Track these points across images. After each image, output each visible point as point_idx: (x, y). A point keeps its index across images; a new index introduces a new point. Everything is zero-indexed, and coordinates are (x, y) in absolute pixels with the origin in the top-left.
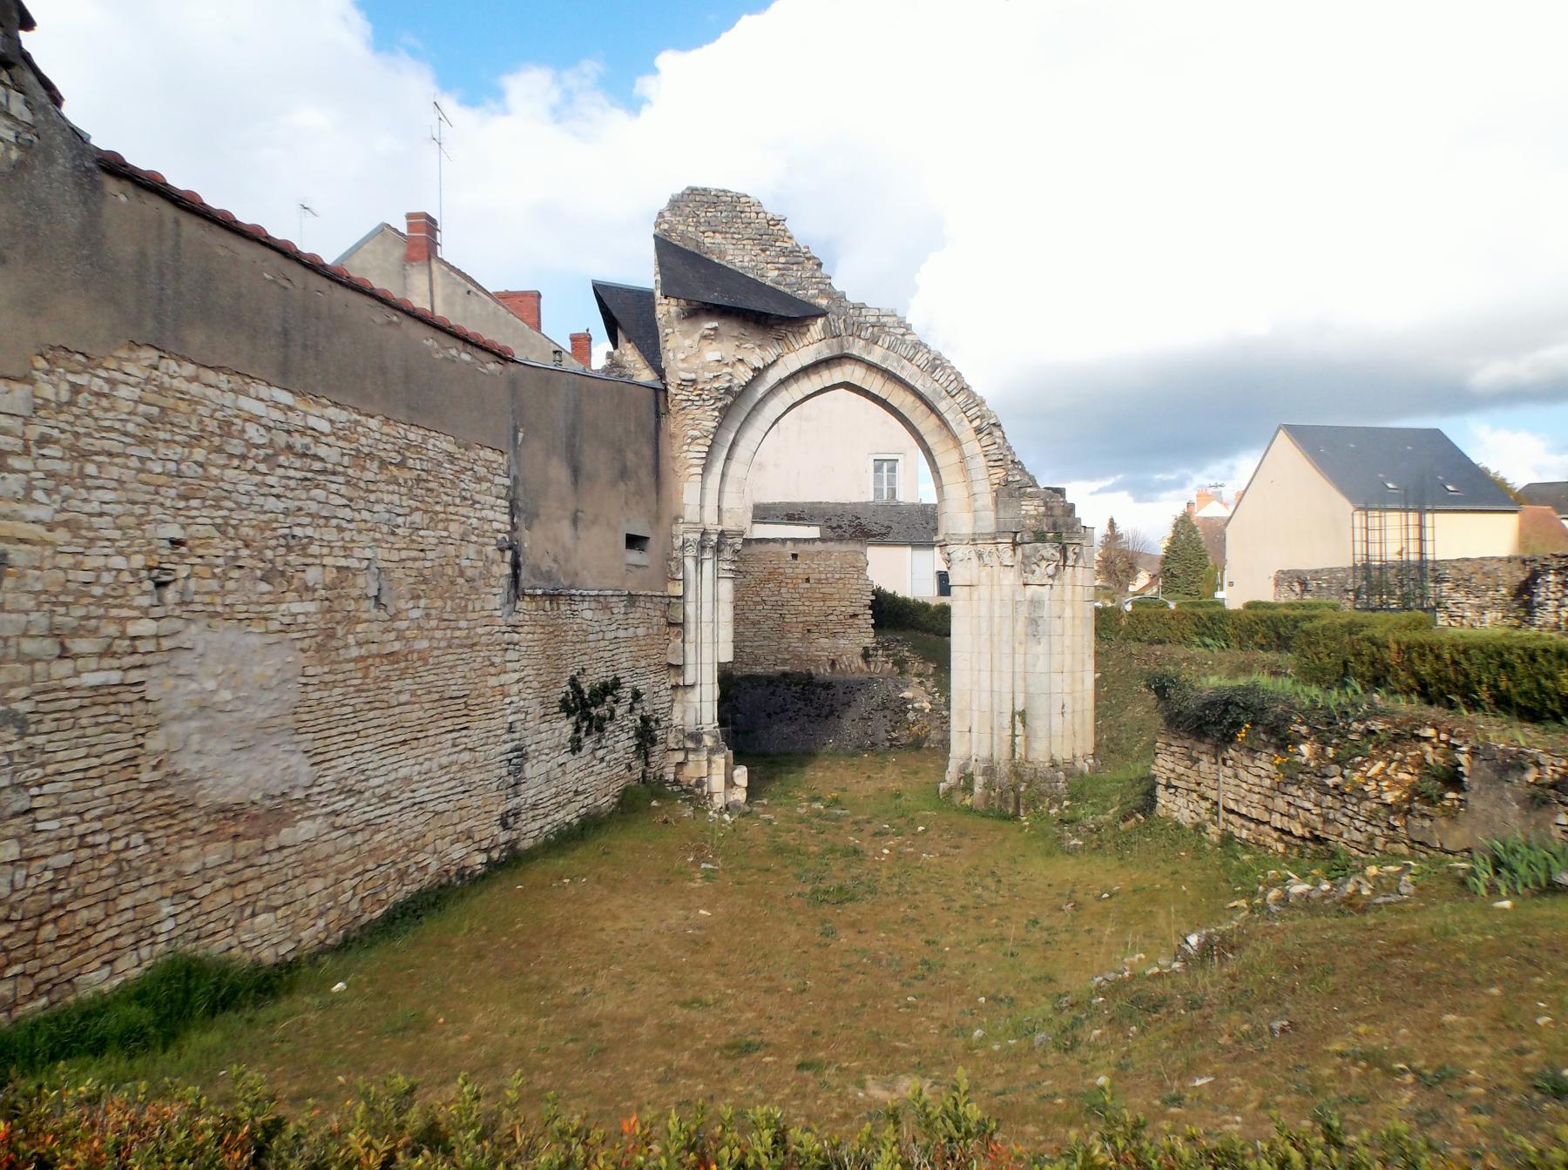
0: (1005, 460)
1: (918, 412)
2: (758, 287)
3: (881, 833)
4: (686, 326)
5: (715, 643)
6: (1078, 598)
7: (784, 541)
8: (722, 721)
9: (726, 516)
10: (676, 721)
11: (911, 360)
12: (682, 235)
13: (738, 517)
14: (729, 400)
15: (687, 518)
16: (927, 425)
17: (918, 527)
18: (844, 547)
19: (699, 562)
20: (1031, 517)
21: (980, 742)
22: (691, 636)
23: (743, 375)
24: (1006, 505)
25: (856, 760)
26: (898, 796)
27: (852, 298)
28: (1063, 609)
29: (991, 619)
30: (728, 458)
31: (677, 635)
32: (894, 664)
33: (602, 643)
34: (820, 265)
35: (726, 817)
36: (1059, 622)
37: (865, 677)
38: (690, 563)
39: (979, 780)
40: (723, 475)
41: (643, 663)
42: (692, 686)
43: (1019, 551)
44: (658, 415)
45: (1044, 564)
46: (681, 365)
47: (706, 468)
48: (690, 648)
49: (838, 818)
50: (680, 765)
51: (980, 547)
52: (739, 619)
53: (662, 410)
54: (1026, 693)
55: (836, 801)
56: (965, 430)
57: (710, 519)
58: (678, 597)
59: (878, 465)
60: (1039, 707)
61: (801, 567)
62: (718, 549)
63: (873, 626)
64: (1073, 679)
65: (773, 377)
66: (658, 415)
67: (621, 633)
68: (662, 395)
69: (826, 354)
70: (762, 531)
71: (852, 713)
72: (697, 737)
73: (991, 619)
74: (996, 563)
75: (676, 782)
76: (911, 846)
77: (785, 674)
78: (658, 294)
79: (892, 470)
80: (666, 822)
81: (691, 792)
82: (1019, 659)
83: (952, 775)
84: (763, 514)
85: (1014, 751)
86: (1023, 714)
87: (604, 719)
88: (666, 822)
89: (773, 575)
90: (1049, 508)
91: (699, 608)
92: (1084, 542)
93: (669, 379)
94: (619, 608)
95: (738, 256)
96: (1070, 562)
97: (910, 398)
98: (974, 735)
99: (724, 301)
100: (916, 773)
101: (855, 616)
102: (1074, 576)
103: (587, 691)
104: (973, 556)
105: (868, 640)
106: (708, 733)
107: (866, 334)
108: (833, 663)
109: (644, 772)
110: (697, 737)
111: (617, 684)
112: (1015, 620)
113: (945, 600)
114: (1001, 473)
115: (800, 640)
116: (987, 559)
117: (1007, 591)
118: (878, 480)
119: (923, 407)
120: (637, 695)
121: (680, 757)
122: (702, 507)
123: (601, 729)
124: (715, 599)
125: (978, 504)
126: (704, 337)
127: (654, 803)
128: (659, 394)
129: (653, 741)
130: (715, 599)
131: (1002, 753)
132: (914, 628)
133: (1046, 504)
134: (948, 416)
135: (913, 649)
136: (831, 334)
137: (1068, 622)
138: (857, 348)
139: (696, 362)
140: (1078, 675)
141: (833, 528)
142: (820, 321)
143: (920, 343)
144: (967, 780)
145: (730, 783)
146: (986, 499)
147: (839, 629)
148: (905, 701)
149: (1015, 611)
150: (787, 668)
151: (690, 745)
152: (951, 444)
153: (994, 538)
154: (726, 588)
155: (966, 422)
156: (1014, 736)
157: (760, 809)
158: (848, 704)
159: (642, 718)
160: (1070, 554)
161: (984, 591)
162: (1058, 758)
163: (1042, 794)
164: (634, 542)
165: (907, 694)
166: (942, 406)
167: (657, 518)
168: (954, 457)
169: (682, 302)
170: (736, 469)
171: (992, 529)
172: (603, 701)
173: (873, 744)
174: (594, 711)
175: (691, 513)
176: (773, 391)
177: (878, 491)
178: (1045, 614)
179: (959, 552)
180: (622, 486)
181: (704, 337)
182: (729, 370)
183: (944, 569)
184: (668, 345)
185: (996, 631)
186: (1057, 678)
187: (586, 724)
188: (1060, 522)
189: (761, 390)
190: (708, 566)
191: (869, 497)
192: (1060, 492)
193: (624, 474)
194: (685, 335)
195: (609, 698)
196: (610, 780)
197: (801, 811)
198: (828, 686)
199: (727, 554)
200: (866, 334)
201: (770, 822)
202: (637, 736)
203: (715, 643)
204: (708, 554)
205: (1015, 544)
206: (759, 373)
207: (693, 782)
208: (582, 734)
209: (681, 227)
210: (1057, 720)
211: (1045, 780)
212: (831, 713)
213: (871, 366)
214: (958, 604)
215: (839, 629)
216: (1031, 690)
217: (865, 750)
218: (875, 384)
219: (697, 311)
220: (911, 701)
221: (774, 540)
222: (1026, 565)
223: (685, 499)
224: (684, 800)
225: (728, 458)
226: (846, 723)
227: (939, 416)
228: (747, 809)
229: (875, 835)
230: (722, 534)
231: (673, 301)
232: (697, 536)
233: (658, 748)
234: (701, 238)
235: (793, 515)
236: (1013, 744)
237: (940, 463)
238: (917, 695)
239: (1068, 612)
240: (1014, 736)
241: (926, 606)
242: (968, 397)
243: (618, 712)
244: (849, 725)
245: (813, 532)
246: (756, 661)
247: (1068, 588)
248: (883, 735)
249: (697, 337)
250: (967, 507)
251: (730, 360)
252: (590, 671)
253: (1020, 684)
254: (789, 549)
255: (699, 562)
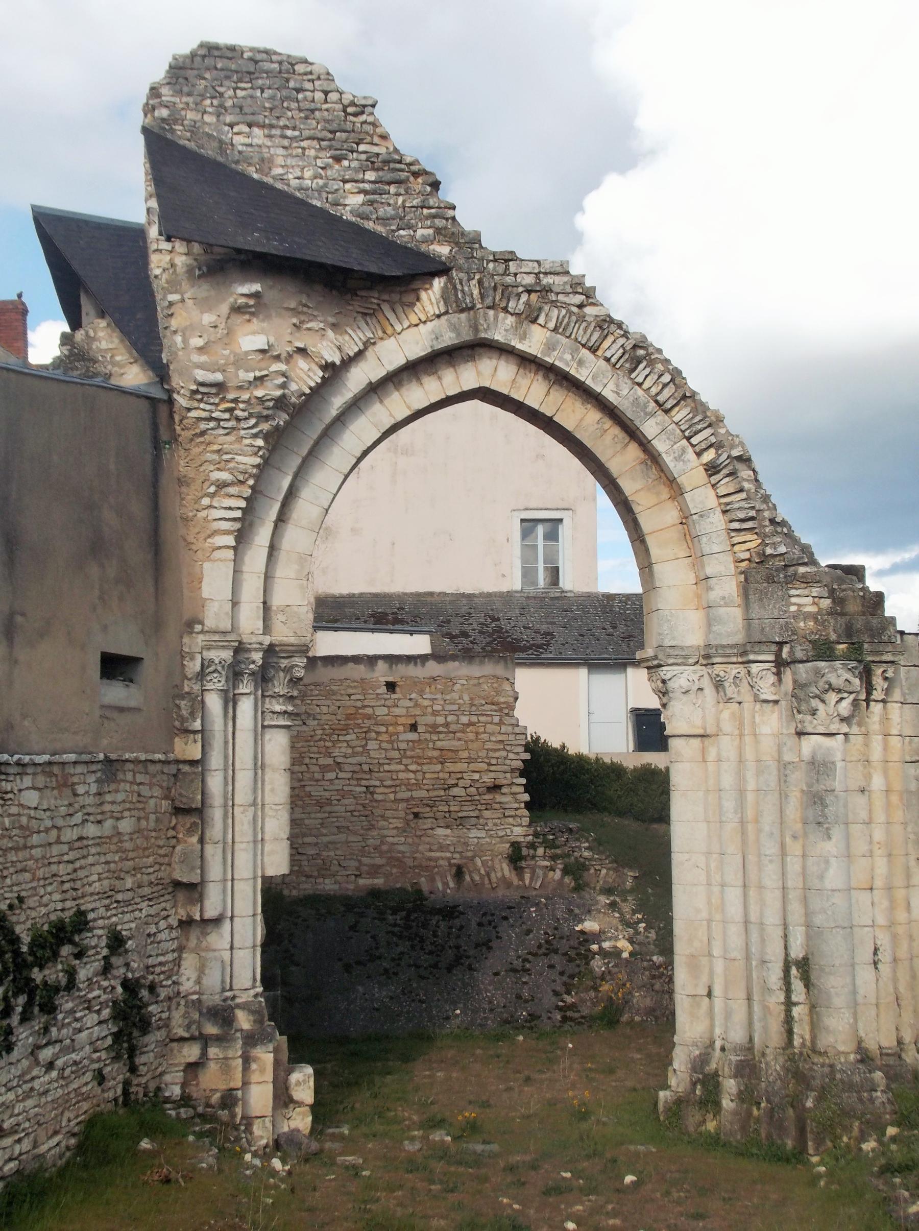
0: (756, 516)
1: (608, 438)
2: (328, 222)
3: (558, 1190)
4: (204, 290)
5: (258, 841)
6: (895, 757)
7: (372, 660)
8: (268, 980)
9: (278, 620)
10: (187, 985)
11: (594, 350)
12: (194, 129)
13: (293, 625)
14: (282, 418)
15: (210, 623)
16: (622, 460)
17: (610, 634)
18: (475, 670)
19: (230, 700)
20: (807, 616)
21: (728, 1015)
22: (215, 830)
23: (306, 375)
24: (763, 596)
25: (503, 1048)
26: (583, 1116)
27: (492, 243)
28: (868, 777)
29: (741, 792)
30: (281, 519)
31: (190, 831)
32: (566, 871)
33: (56, 850)
34: (436, 185)
35: (277, 1163)
36: (860, 801)
37: (513, 896)
38: (214, 702)
39: (730, 1085)
40: (273, 548)
41: (129, 882)
42: (217, 921)
43: (788, 676)
44: (157, 445)
45: (832, 697)
46: (196, 358)
47: (242, 537)
48: (213, 853)
49: (477, 1161)
50: (193, 1068)
51: (718, 669)
52: (299, 798)
53: (164, 435)
54: (808, 926)
55: (473, 1128)
56: (688, 468)
57: (249, 622)
58: (193, 763)
59: (528, 526)
60: (834, 950)
61: (403, 706)
62: (263, 678)
63: (528, 806)
64: (892, 901)
65: (358, 378)
66: (157, 445)
67: (91, 830)
68: (163, 409)
69: (449, 339)
70: (332, 643)
71: (494, 961)
72: (223, 1015)
73: (741, 792)
74: (747, 697)
75: (185, 1100)
76: (615, 1214)
77: (375, 893)
78: (153, 232)
79: (552, 536)
80: (167, 1181)
81: (213, 1118)
82: (794, 865)
83: (679, 1075)
84: (334, 612)
85: (790, 1032)
86: (804, 965)
87: (57, 989)
88: (167, 1181)
89: (355, 721)
90: (838, 601)
91: (230, 780)
92: (902, 660)
93: (176, 381)
94: (87, 786)
95: (296, 169)
96: (877, 695)
97: (593, 416)
98: (718, 1003)
99: (273, 247)
100: (611, 1071)
101: (495, 788)
102: (885, 719)
103: (26, 939)
104: (706, 683)
105: (519, 829)
106: (244, 1006)
107: (518, 305)
108: (459, 873)
109: (127, 1084)
110: (223, 1015)
111: (81, 922)
112: (783, 796)
113: (655, 759)
114: (753, 542)
115: (402, 831)
116: (730, 690)
117: (768, 747)
118: (529, 550)
119: (616, 431)
120: (117, 942)
121: (192, 1052)
122: (235, 603)
123: (49, 1008)
124: (259, 766)
125: (714, 595)
126: (237, 310)
127: (145, 1144)
128: (159, 408)
129: (145, 1026)
130: (259, 766)
131: (770, 1034)
132: (600, 808)
133: (832, 594)
134: (660, 445)
135: (598, 845)
136: (455, 303)
137: (879, 802)
138: (501, 329)
139: (223, 354)
140: (900, 894)
141: (452, 637)
142: (438, 283)
143: (612, 321)
144: (707, 1084)
145: (283, 1098)
146: (727, 587)
147: (468, 811)
148: (587, 938)
149: (783, 779)
150: (379, 882)
151: (211, 1029)
152: (665, 493)
153: (743, 653)
154: (277, 746)
155: (690, 454)
156: (789, 1004)
157: (337, 1146)
158: (486, 945)
159: (125, 984)
160: (878, 682)
161: (727, 746)
162: (872, 1045)
163: (847, 1113)
164: (115, 666)
165: (590, 925)
166: (650, 428)
167: (155, 625)
168: (671, 515)
169: (197, 248)
170: (295, 537)
171: (739, 638)
172: (56, 955)
173: (533, 1017)
174: (37, 975)
175: (215, 615)
176: (356, 405)
177: (528, 573)
178: (838, 785)
179: (682, 677)
180: (94, 571)
181: (237, 310)
182: (282, 367)
183: (653, 702)
184: (174, 323)
185: (750, 814)
186: (864, 898)
187: (22, 1000)
188: (859, 624)
189: (337, 402)
190: (246, 707)
191: (514, 583)
192: (857, 572)
193: (97, 547)
194: (205, 305)
195: (66, 950)
196: (63, 1104)
197: (409, 1147)
198: (450, 912)
199: (280, 686)
200: (518, 305)
201: (355, 1170)
202: (115, 1017)
203: (258, 841)
204: (246, 687)
205: (780, 664)
206: (333, 373)
207: (216, 1098)
208: (15, 1020)
209: (191, 115)
210: (865, 975)
211: (850, 1086)
212: (458, 960)
213: (526, 361)
214: (683, 765)
215: (468, 811)
216: (818, 920)
217: (519, 1029)
218: (534, 392)
219: (222, 263)
220: (597, 937)
221: (356, 659)
222: (801, 700)
223: (207, 591)
224: (200, 1135)
225: (281, 519)
226: (483, 978)
227: (644, 444)
228: (315, 1146)
229: (547, 1192)
230: (270, 651)
231: (180, 247)
232: (227, 655)
233: (154, 1038)
234: (227, 134)
235: (384, 614)
236: (789, 1020)
237: (646, 523)
238: (608, 929)
239: (877, 782)
240: (789, 1004)
241: (615, 771)
242: (695, 411)
243: (83, 974)
244: (490, 987)
245: (420, 644)
246: (324, 870)
247: (877, 742)
248: (549, 1000)
249: (224, 309)
250: (695, 604)
251: (284, 349)
252: (31, 902)
253: (796, 911)
254: (382, 674)
255: (230, 700)
